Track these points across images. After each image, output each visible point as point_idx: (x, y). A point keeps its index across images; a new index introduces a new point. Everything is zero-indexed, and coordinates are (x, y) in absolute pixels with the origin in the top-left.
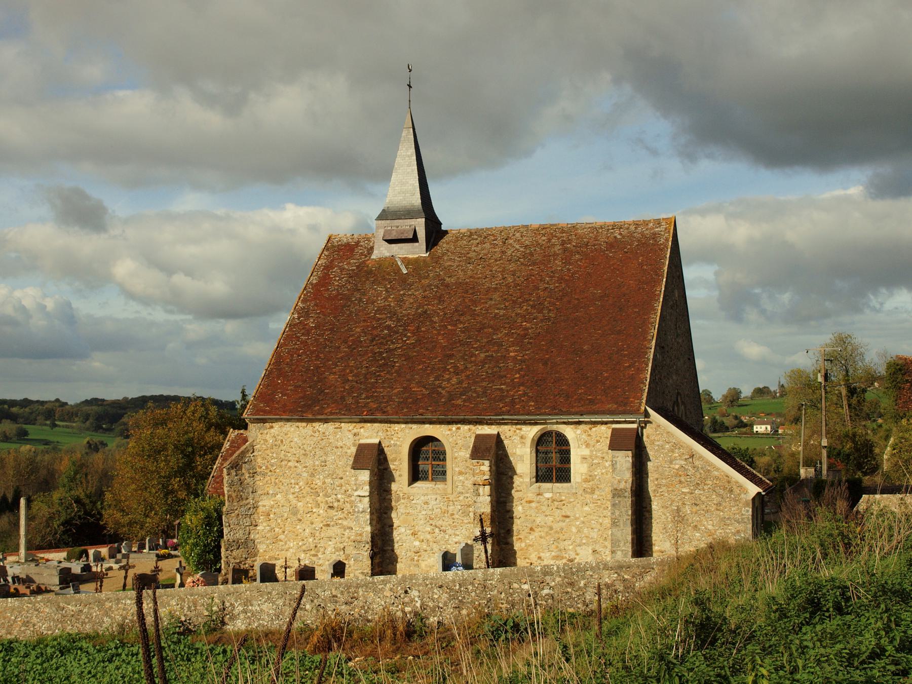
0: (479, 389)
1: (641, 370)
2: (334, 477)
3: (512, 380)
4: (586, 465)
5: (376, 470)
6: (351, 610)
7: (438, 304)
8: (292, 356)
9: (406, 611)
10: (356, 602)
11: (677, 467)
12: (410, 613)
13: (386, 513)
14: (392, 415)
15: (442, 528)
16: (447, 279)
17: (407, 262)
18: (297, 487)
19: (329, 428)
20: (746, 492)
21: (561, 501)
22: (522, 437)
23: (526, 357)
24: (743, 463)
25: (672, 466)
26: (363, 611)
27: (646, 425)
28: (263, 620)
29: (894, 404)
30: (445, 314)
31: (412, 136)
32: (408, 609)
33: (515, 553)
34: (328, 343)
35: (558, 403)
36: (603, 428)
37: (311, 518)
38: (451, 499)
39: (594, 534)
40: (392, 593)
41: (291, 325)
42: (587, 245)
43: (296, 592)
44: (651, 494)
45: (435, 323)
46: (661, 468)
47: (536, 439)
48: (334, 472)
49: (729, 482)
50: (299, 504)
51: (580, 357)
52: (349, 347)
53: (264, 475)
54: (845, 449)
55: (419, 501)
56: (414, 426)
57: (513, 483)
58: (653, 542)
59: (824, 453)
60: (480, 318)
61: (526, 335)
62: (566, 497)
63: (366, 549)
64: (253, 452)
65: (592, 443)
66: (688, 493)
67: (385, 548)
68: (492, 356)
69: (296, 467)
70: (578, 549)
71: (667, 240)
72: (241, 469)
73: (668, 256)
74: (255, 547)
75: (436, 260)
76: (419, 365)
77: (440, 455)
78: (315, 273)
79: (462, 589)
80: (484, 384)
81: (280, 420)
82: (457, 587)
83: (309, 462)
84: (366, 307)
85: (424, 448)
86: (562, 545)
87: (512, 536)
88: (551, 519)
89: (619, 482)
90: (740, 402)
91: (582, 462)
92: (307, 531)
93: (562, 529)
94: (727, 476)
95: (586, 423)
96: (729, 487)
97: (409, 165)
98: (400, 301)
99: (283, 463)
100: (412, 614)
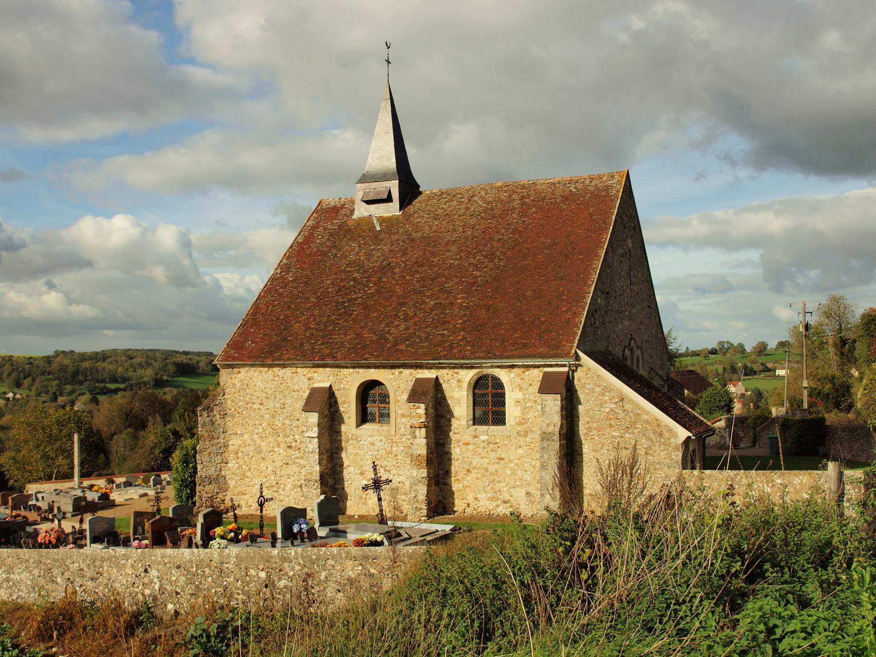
1: (577, 314)
2: (292, 418)
4: (519, 408)
5: (327, 412)
6: (96, 588)
7: (401, 257)
8: (268, 307)
9: (146, 593)
11: (607, 410)
12: (149, 596)
14: (341, 359)
15: (387, 468)
16: (414, 234)
17: (381, 220)
18: (261, 427)
20: (675, 436)
21: (496, 443)
22: (459, 381)
24: (685, 406)
25: (602, 409)
26: (106, 590)
27: (577, 368)
28: (22, 591)
29: (867, 350)
30: (406, 266)
31: (390, 107)
32: (147, 592)
33: (453, 493)
34: (300, 295)
36: (536, 371)
37: (273, 457)
38: (394, 441)
39: (527, 477)
40: (133, 571)
41: (273, 279)
42: (544, 199)
43: (49, 561)
44: (582, 437)
45: (396, 274)
46: (591, 411)
47: (473, 382)
48: (292, 414)
49: (659, 426)
50: (263, 443)
51: (521, 302)
52: (317, 298)
53: (233, 416)
54: (825, 390)
55: (366, 442)
56: (361, 371)
57: (451, 425)
58: (584, 485)
59: (805, 393)
60: (436, 269)
63: (315, 487)
64: (224, 395)
65: (525, 386)
66: (618, 436)
67: (337, 487)
68: (441, 303)
69: (259, 409)
70: (512, 490)
71: (618, 191)
72: (212, 410)
73: (617, 206)
75: (407, 217)
76: (374, 313)
77: (385, 398)
78: (302, 233)
79: (199, 572)
80: (428, 330)
82: (194, 569)
83: (271, 405)
84: (339, 262)
85: (372, 392)
86: (497, 486)
87: (450, 477)
88: (487, 461)
89: (548, 425)
90: (766, 352)
91: (516, 406)
92: (270, 468)
93: (497, 471)
94: (657, 420)
96: (659, 431)
98: (369, 255)
99: (249, 405)
100: (151, 599)
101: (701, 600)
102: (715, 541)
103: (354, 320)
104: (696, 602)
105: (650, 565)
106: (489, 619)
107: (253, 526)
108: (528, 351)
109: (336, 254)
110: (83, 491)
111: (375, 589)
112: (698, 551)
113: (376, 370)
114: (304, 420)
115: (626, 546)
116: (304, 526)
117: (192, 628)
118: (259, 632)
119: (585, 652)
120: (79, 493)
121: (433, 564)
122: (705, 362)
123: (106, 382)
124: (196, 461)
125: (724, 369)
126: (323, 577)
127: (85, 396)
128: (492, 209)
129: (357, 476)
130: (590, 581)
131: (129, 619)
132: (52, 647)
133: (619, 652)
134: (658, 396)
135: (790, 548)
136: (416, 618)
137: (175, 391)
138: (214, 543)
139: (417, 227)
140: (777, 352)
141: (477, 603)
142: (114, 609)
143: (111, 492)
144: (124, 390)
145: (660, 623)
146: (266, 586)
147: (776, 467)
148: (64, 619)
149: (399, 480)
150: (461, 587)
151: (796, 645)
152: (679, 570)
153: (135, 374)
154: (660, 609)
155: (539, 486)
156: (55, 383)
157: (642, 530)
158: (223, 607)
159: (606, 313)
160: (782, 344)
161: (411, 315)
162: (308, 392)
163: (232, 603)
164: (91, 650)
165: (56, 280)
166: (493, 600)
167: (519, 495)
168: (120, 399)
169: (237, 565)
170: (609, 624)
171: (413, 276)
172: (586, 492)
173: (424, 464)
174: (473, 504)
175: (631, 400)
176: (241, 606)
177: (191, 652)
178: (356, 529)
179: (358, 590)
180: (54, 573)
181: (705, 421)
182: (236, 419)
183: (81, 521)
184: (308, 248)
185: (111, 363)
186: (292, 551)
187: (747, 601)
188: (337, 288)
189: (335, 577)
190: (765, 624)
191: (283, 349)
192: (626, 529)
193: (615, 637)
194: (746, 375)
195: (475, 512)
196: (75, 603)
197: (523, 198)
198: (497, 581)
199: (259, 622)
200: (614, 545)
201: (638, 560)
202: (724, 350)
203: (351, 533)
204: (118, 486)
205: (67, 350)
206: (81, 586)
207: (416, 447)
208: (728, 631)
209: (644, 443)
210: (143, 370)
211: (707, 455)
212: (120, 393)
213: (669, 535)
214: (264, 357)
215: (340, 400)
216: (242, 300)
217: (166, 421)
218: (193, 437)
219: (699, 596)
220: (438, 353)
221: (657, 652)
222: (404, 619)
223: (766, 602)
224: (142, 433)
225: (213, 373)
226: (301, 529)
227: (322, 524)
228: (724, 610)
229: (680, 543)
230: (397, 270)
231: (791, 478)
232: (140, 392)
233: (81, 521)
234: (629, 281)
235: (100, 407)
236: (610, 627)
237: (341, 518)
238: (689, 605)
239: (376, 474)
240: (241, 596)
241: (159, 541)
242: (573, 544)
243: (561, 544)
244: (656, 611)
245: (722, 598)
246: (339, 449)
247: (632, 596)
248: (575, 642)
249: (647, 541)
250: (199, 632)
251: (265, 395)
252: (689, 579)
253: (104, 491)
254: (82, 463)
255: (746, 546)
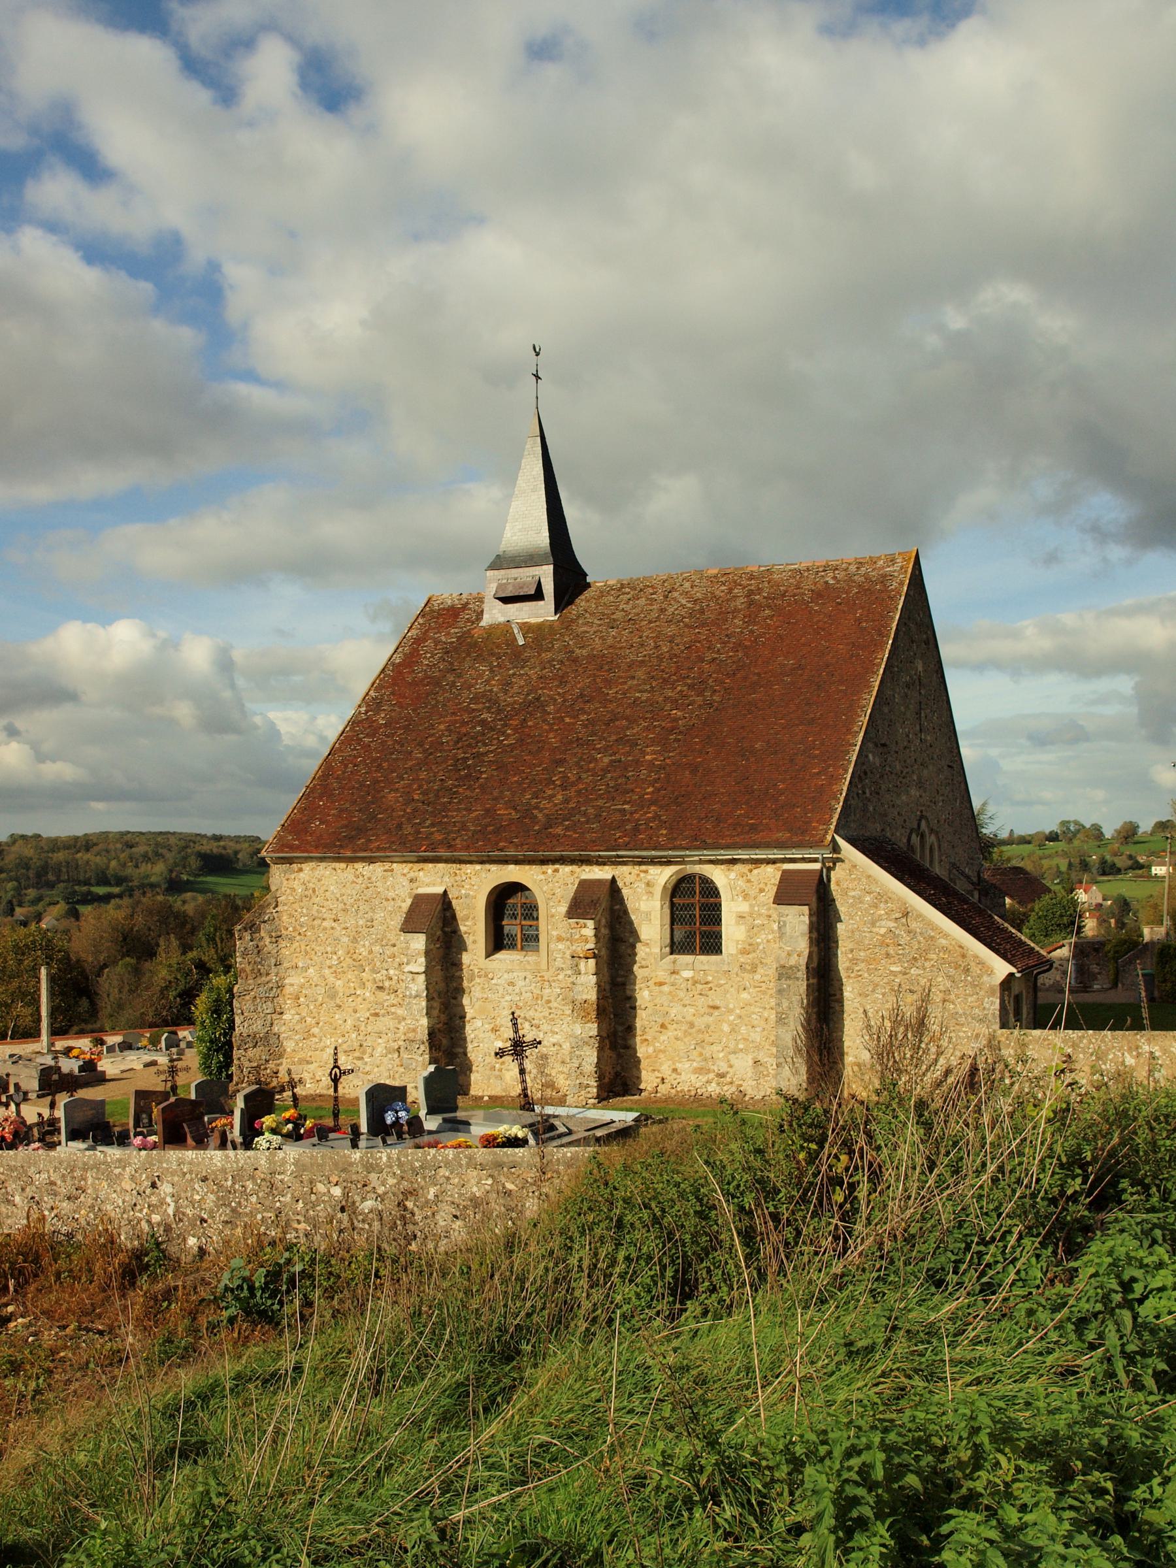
0: (591, 811)
1: (836, 779)
3: (641, 797)
4: (743, 928)
5: (439, 933)
6: (75, 1212)
7: (558, 687)
8: (346, 766)
10: (82, 1198)
11: (883, 931)
12: (159, 1224)
13: (455, 998)
14: (460, 850)
16: (578, 651)
17: (526, 628)
18: (335, 957)
19: (376, 870)
20: (990, 972)
21: (707, 983)
22: (648, 884)
23: (668, 761)
24: (1006, 925)
25: (874, 930)
27: (834, 864)
30: (564, 701)
32: (156, 1218)
33: (639, 1061)
35: (703, 831)
36: (770, 869)
39: (756, 1036)
40: (134, 1186)
41: (354, 723)
42: (783, 595)
44: (843, 974)
45: (549, 714)
47: (670, 887)
49: (964, 956)
50: (339, 983)
51: (748, 760)
53: (291, 939)
55: (500, 981)
56: (494, 868)
57: (635, 954)
58: (846, 1050)
61: (673, 728)
62: (714, 977)
63: (420, 1051)
64: (277, 906)
65: (752, 893)
68: (620, 761)
69: (332, 928)
70: (732, 1057)
71: (901, 584)
73: (900, 607)
74: (280, 1044)
75: (567, 625)
76: (515, 775)
77: (531, 912)
78: (400, 649)
79: (237, 1186)
80: (600, 803)
81: (310, 859)
82: (229, 1183)
83: (351, 922)
85: (511, 901)
86: (708, 1051)
87: (635, 1036)
88: (692, 1010)
89: (789, 955)
90: (1136, 838)
91: (738, 923)
92: (349, 1022)
93: (708, 1027)
94: (960, 947)
95: (743, 861)
96: (963, 964)
97: (534, 490)
98: (506, 684)
99: (316, 922)
100: (162, 1229)
101: (1020, 1238)
102: (1042, 1143)
103: (482, 787)
104: (1012, 1240)
105: (940, 1180)
106: (690, 1265)
107: (323, 1113)
108: (757, 837)
109: (454, 682)
110: (55, 1058)
111: (514, 1215)
112: (1017, 1160)
113: (518, 867)
114: (404, 945)
115: (903, 1152)
116: (402, 1114)
117: (226, 1275)
118: (331, 1283)
119: (838, 1317)
120: (49, 1061)
121: (599, 1176)
122: (1040, 853)
123: (91, 885)
124: (232, 1010)
125: (1070, 865)
126: (431, 1196)
127: (58, 906)
128: (702, 612)
129: (487, 1035)
130: (848, 1206)
131: (127, 1260)
132: (6, 1305)
133: (889, 1319)
134: (964, 910)
135: (1160, 1155)
136: (576, 1263)
137: (200, 898)
138: (261, 1141)
139: (581, 640)
140: (1152, 838)
141: (670, 1240)
142: (105, 1245)
143: (100, 1060)
144: (120, 896)
145: (955, 1272)
146: (343, 1210)
147: (1138, 1026)
148: (25, 1261)
149: (553, 1040)
150: (645, 1215)
151: (1166, 1310)
152: (986, 1189)
153: (138, 871)
154: (956, 1251)
155: (774, 1050)
156: (10, 885)
157: (928, 1126)
158: (275, 1242)
159: (882, 776)
160: (1162, 826)
161: (573, 779)
162: (409, 901)
163: (288, 1236)
164: (68, 1310)
165: (20, 723)
166: (695, 1235)
167: (742, 1066)
168: (115, 912)
169: (297, 1176)
170: (875, 1275)
171: (576, 717)
172: (849, 1059)
173: (593, 1015)
174: (671, 1078)
175: (920, 916)
176: (303, 1240)
177: (224, 1313)
178: (485, 1119)
179: (487, 1216)
180: (9, 1189)
181: (1037, 948)
182: (296, 945)
183: (52, 1106)
184: (409, 673)
185: (98, 854)
186: (384, 1155)
187: (1092, 1239)
188: (454, 737)
189: (451, 1196)
190: (1118, 1276)
191: (371, 833)
192: (905, 1124)
193: (884, 1294)
194: (1104, 874)
195: (673, 1091)
196: (43, 1235)
197: (751, 593)
198: (701, 1206)
199: (331, 1266)
200: (885, 1150)
201: (923, 1173)
202: (1070, 835)
203: (477, 1124)
204: (111, 1049)
205: (30, 834)
206: (52, 1208)
207: (578, 988)
208: (1059, 1287)
209: (942, 982)
210: (149, 865)
211: (1040, 1001)
212: (113, 901)
213: (971, 1135)
214: (341, 846)
215: (459, 914)
216: (309, 754)
217: (186, 948)
218: (229, 972)
219: (1016, 1230)
220: (616, 840)
221: (949, 1319)
222: (556, 1265)
223: (1119, 1242)
224: (147, 965)
225: (259, 869)
226: (398, 1118)
227: (431, 1111)
228: (1055, 1253)
229: (988, 1146)
230: (551, 708)
231: (1168, 1043)
232: (144, 900)
233: (52, 1106)
234: (918, 728)
235: (83, 923)
236: (878, 1279)
237: (461, 1100)
238: (1001, 1244)
239: (516, 1032)
240: (303, 1226)
241: (174, 1137)
242: (822, 1147)
243: (802, 1147)
244: (949, 1254)
245: (1053, 1234)
246: (459, 991)
247: (912, 1231)
248: (823, 1302)
249: (937, 1144)
250: (238, 1282)
251: (341, 906)
252: (1001, 1204)
253: (88, 1056)
254: (52, 1014)
255: (1089, 1154)
